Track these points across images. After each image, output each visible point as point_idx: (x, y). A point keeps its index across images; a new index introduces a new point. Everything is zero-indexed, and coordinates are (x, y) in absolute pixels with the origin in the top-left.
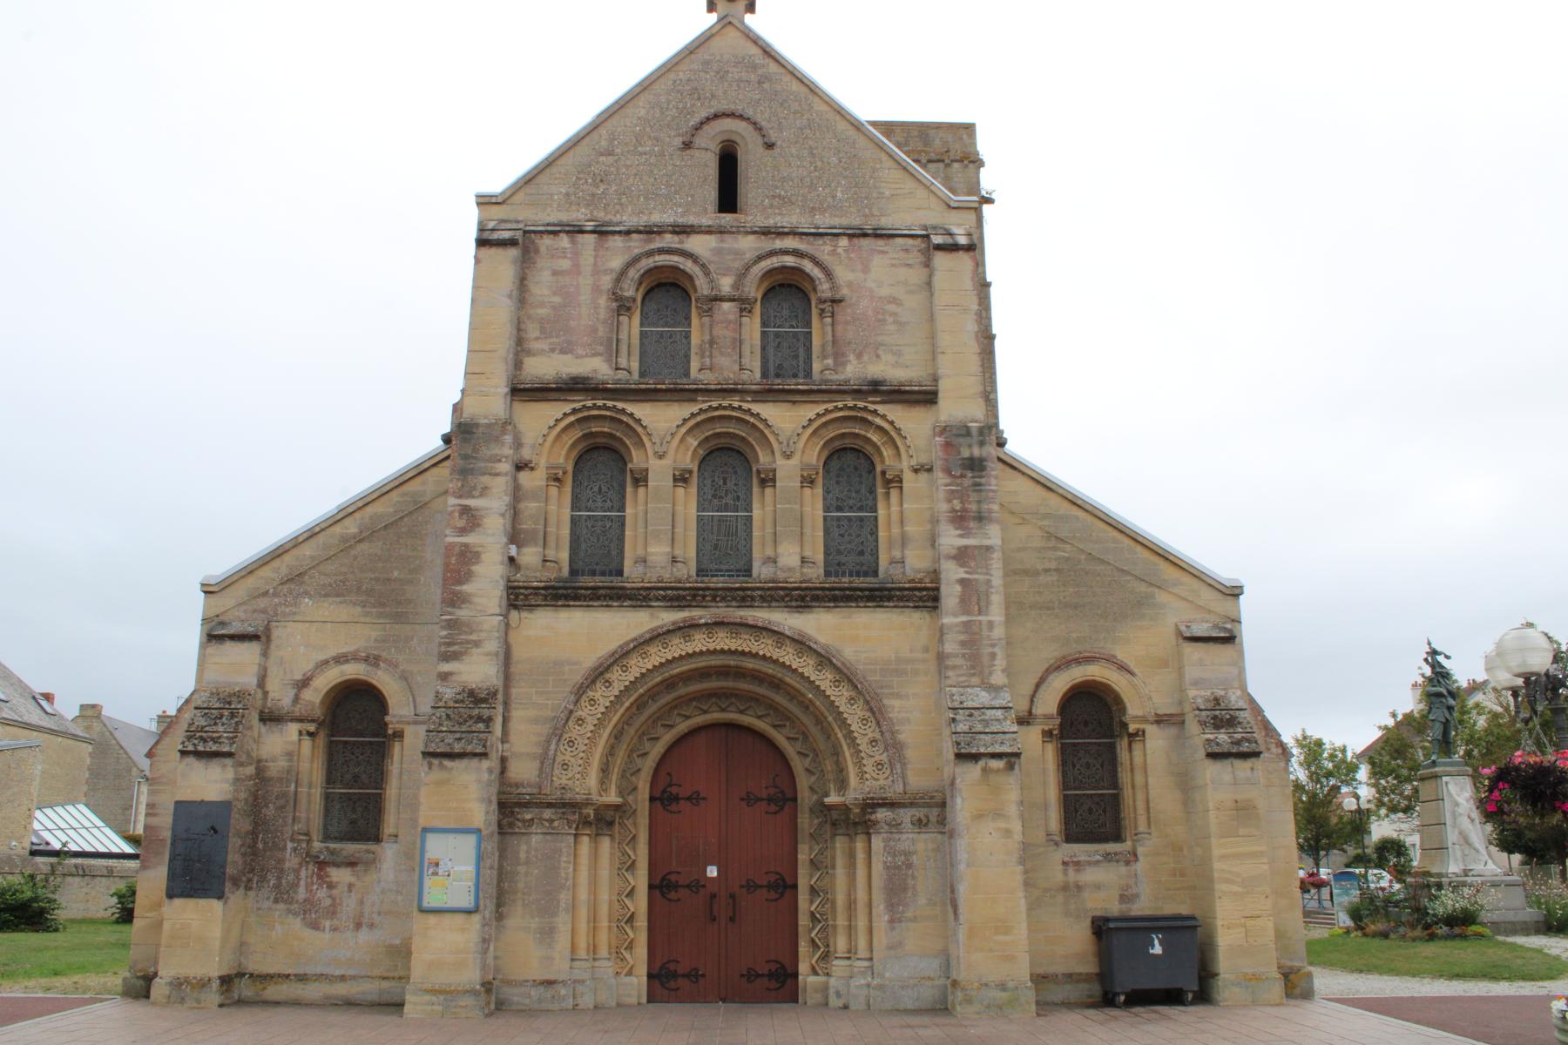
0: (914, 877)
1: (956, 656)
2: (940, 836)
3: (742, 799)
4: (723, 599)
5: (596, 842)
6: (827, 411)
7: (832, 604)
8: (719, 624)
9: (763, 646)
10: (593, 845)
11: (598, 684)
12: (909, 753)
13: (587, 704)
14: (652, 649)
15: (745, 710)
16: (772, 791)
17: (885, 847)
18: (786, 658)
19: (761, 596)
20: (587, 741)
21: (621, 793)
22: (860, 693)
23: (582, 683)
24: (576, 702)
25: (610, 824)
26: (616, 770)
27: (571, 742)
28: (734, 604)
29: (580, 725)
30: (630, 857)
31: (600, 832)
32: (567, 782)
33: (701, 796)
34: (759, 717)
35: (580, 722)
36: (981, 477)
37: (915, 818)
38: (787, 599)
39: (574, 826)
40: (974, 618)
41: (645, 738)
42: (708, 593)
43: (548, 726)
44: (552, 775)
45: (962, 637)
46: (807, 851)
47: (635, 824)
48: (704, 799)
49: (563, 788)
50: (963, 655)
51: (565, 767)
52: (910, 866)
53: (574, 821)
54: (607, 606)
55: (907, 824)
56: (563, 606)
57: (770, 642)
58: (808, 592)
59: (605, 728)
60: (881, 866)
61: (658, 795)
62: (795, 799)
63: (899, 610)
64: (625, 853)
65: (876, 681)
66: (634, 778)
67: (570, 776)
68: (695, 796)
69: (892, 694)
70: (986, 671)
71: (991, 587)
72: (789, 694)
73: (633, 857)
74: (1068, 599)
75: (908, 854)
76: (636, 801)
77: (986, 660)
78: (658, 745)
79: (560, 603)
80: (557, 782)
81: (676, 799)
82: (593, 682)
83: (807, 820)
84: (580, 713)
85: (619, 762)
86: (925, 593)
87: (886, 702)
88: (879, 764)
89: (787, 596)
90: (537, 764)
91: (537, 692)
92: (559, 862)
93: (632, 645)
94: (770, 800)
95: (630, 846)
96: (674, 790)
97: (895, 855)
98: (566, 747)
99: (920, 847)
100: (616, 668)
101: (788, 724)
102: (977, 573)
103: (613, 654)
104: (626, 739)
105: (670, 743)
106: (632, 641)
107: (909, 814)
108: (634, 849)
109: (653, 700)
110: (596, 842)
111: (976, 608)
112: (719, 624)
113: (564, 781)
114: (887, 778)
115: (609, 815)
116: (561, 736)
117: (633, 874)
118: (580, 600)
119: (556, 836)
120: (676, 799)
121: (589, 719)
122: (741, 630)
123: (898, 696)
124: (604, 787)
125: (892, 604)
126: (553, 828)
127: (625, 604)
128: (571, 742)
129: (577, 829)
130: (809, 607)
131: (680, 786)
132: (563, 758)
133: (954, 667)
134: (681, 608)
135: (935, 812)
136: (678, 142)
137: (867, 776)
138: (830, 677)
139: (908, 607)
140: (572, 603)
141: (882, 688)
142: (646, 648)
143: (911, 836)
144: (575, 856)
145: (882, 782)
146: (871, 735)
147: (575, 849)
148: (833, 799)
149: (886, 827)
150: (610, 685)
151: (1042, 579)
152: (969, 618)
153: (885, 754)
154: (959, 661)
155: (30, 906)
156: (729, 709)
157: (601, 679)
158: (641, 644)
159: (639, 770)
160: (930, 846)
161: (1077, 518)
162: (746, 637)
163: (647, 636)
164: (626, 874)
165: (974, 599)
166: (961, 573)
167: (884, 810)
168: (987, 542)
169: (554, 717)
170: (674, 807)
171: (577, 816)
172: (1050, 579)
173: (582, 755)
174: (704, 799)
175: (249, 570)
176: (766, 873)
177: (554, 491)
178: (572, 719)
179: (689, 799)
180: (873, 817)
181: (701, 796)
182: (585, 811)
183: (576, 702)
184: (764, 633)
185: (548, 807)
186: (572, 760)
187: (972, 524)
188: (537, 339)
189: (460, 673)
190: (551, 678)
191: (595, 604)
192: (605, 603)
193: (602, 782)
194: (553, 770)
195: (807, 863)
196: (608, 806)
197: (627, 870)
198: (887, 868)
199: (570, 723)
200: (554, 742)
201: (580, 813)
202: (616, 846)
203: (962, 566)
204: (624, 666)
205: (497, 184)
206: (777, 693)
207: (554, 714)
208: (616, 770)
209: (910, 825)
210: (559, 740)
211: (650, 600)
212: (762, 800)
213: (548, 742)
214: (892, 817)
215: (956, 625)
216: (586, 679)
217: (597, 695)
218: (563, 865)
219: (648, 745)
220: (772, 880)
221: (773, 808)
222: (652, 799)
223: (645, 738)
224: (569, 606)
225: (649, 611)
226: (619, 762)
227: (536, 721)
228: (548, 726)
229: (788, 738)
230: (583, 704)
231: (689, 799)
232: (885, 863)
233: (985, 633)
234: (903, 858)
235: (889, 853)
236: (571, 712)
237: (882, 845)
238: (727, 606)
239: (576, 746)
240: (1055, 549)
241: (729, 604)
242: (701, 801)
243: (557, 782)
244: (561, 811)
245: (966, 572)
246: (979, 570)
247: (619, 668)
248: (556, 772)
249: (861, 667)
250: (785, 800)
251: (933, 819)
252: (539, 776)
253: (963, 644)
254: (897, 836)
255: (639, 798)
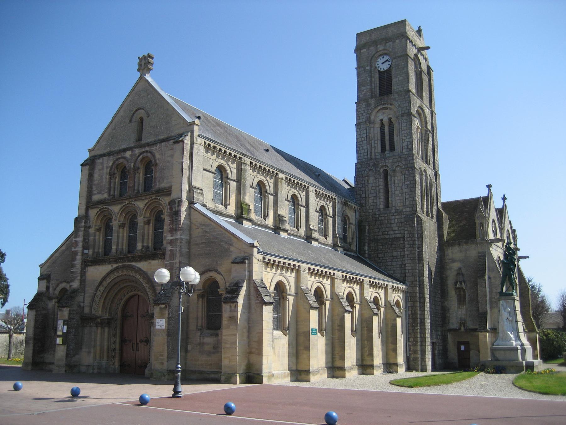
6: (149, 201)
36: (177, 217)
74: (207, 252)
87: (156, 288)
111: (173, 258)
136: (128, 122)
151: (201, 246)
155: (503, 260)
158: (108, 274)
168: (177, 237)
172: (203, 246)
175: (47, 261)
177: (98, 233)
187: (174, 232)
188: (95, 190)
189: (73, 285)
205: (91, 147)
240: (205, 236)
245: (172, 247)
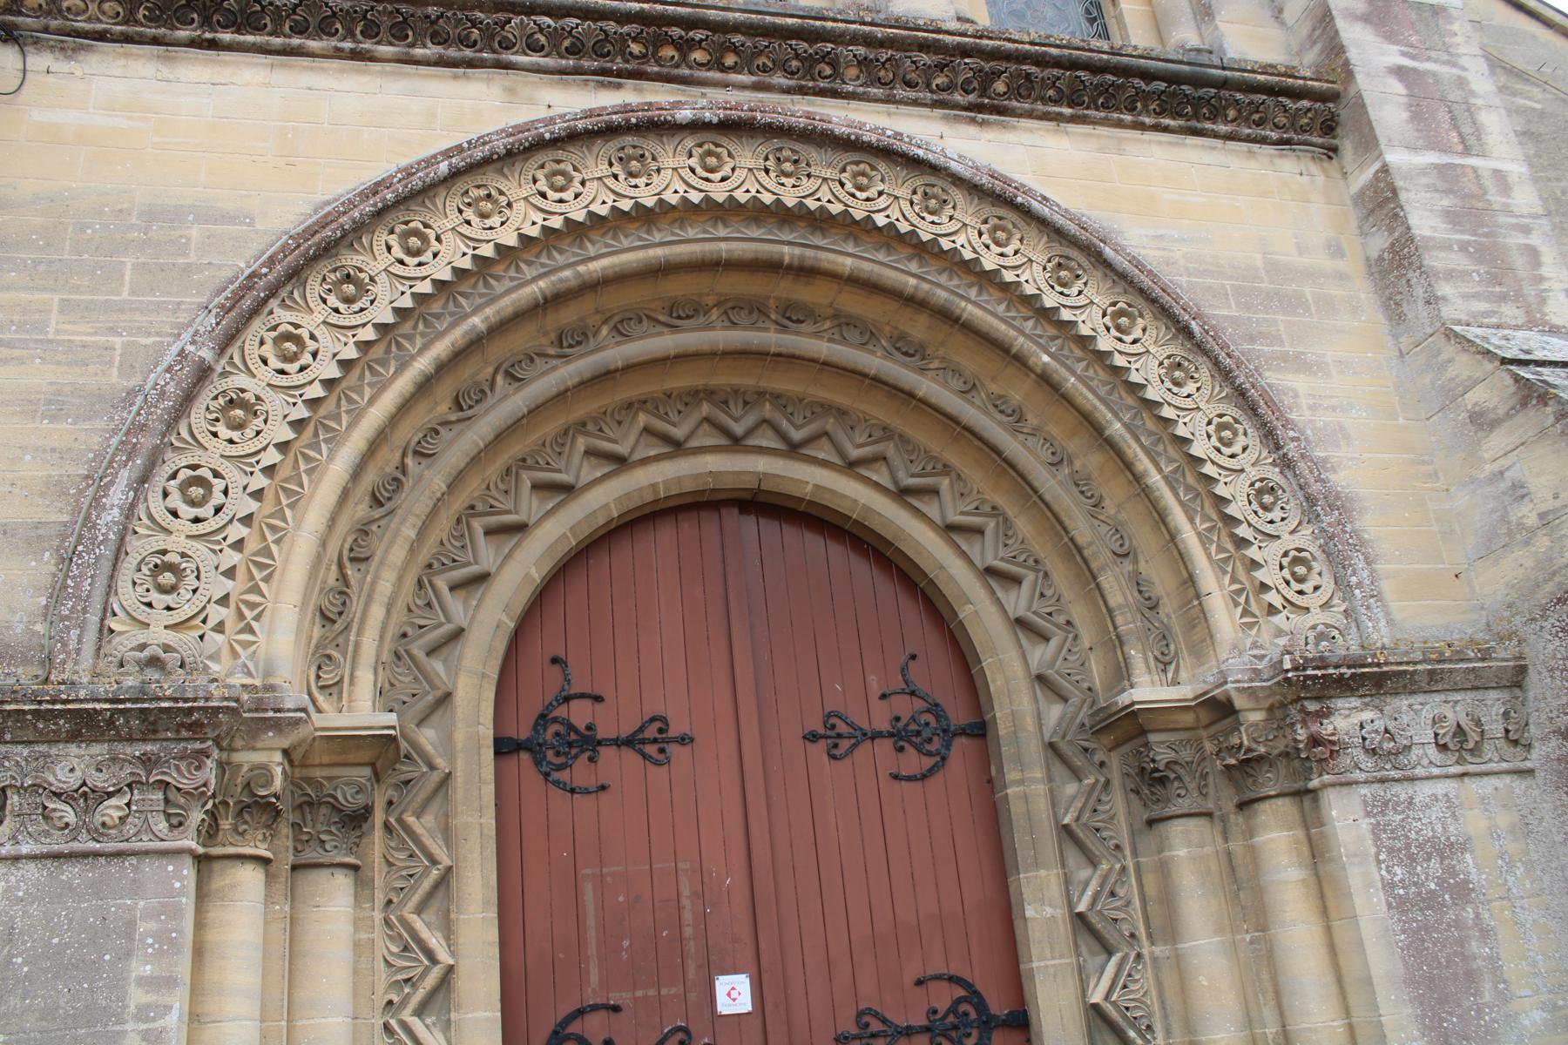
0: (1485, 934)
1: (1446, 247)
2: (1519, 785)
3: (812, 737)
4: (747, 62)
5: (293, 895)
7: (1067, 111)
8: (734, 127)
9: (882, 202)
10: (282, 908)
11: (314, 287)
12: (1371, 525)
13: (268, 350)
14: (516, 187)
15: (806, 442)
16: (905, 707)
17: (1376, 830)
18: (961, 239)
19: (863, 63)
20: (259, 481)
21: (385, 697)
22: (1200, 348)
23: (253, 275)
24: (227, 341)
25: (357, 819)
26: (377, 612)
27: (197, 484)
28: (779, 79)
29: (239, 426)
30: (433, 960)
31: (311, 855)
32: (170, 637)
33: (673, 732)
34: (851, 467)
35: (239, 408)
37: (1447, 729)
38: (940, 80)
39: (196, 816)
40: (1457, 160)
41: (478, 525)
42: (698, 35)
43: (100, 424)
44: (107, 611)
45: (1447, 202)
46: (1054, 888)
47: (447, 833)
48: (683, 740)
49: (154, 662)
50: (1463, 247)
51: (167, 578)
52: (1463, 892)
53: (198, 795)
54: (356, 55)
55: (1425, 755)
56: (193, 43)
57: (905, 192)
58: (1002, 66)
59: (335, 440)
60: (1379, 899)
61: (524, 734)
62: (980, 730)
63: (1244, 146)
64: (412, 944)
65: (1232, 320)
66: (437, 666)
67: (187, 611)
68: (652, 732)
69: (1285, 358)
70: (1530, 291)
71: (1472, 93)
72: (957, 372)
73: (444, 957)
75: (1448, 850)
76: (448, 740)
77: (1519, 262)
78: (520, 555)
79: (183, 34)
80: (127, 638)
81: (588, 742)
82: (295, 275)
83: (1041, 788)
84: (241, 380)
85: (385, 587)
86: (1305, 103)
88: (1297, 560)
89: (941, 67)
90: (44, 566)
91: (66, 307)
92: (118, 985)
93: (443, 168)
94: (901, 736)
95: (430, 915)
96: (580, 713)
97: (1412, 858)
98: (175, 500)
99: (1474, 823)
100: (381, 237)
101: (944, 483)
102: (1429, 59)
103: (375, 189)
104: (415, 503)
105: (562, 550)
106: (447, 154)
107: (1428, 713)
108: (448, 929)
109: (511, 377)
110: (293, 895)
112: (734, 127)
113: (158, 635)
114: (1326, 605)
115: (350, 783)
116: (154, 459)
117: (447, 1026)
118: (258, 29)
119: (114, 868)
120: (588, 742)
121: (275, 403)
122: (809, 153)
123: (1300, 364)
124: (328, 677)
125: (1222, 128)
126: (104, 829)
127: (418, 52)
128: (197, 484)
129: (210, 832)
130: (1001, 111)
131: (598, 699)
132: (160, 541)
133: (1450, 275)
134: (609, 76)
135: (1492, 705)
137: (1273, 598)
138: (1102, 300)
139: (1263, 141)
140: (226, 36)
141: (1252, 339)
142: (494, 181)
143: (1441, 788)
144: (199, 952)
145: (1317, 617)
146: (1254, 474)
147: (200, 925)
148: (1147, 690)
149: (1368, 763)
150: (362, 289)
152: (1445, 159)
153: (1306, 531)
154: (1458, 261)
156: (754, 441)
157: (324, 267)
159: (458, 633)
160: (1504, 820)
161: (1534, 37)
162: (827, 173)
163: (500, 145)
164: (416, 1024)
165: (1442, 115)
166: (1393, 55)
167: (1355, 702)
169: (132, 393)
170: (581, 773)
171: (209, 772)
173: (237, 531)
174: (683, 740)
176: (919, 983)
178: (205, 398)
179: (629, 742)
180: (1326, 728)
181: (673, 732)
182: (246, 758)
183: (227, 341)
184: (882, 166)
185: (74, 737)
186: (199, 550)
190: (129, 261)
191: (313, 44)
192: (348, 45)
193: (322, 659)
194: (110, 589)
195: (1063, 929)
196: (346, 745)
197: (419, 1012)
198: (1399, 905)
199: (198, 417)
200: (124, 476)
201: (222, 766)
202: (378, 916)
203: (1390, 37)
204: (416, 233)
206: (923, 370)
207: (134, 382)
208: (377, 612)
209: (1432, 751)
210: (144, 478)
211: (507, 46)
212: (875, 736)
213: (99, 482)
214: (1379, 725)
215: (1424, 171)
216: (271, 261)
217: (310, 322)
218: (137, 997)
219: (487, 554)
220: (943, 1005)
221: (913, 762)
222: (504, 747)
223: (478, 525)
224: (213, 45)
225: (501, 78)
226: (385, 587)
227: (54, 407)
228: (100, 424)
229: (950, 529)
230: (252, 351)
231: (629, 742)
232: (1389, 886)
233: (1495, 198)
234: (1434, 863)
235: (1391, 851)
236: (203, 373)
237: (1365, 824)
238: (757, 87)
239: (217, 498)
241: (766, 79)
242: (673, 749)
243: (127, 638)
244: (138, 750)
245: (1404, 54)
246: (1433, 54)
247: (393, 240)
248: (127, 595)
249: (1183, 280)
250: (949, 735)
251: (1495, 728)
252: (47, 614)
253: (1452, 217)
254: (1402, 792)
255: (460, 736)
